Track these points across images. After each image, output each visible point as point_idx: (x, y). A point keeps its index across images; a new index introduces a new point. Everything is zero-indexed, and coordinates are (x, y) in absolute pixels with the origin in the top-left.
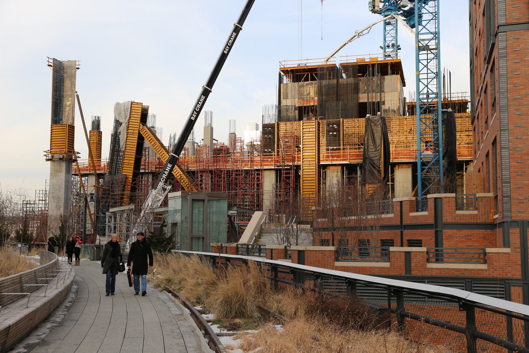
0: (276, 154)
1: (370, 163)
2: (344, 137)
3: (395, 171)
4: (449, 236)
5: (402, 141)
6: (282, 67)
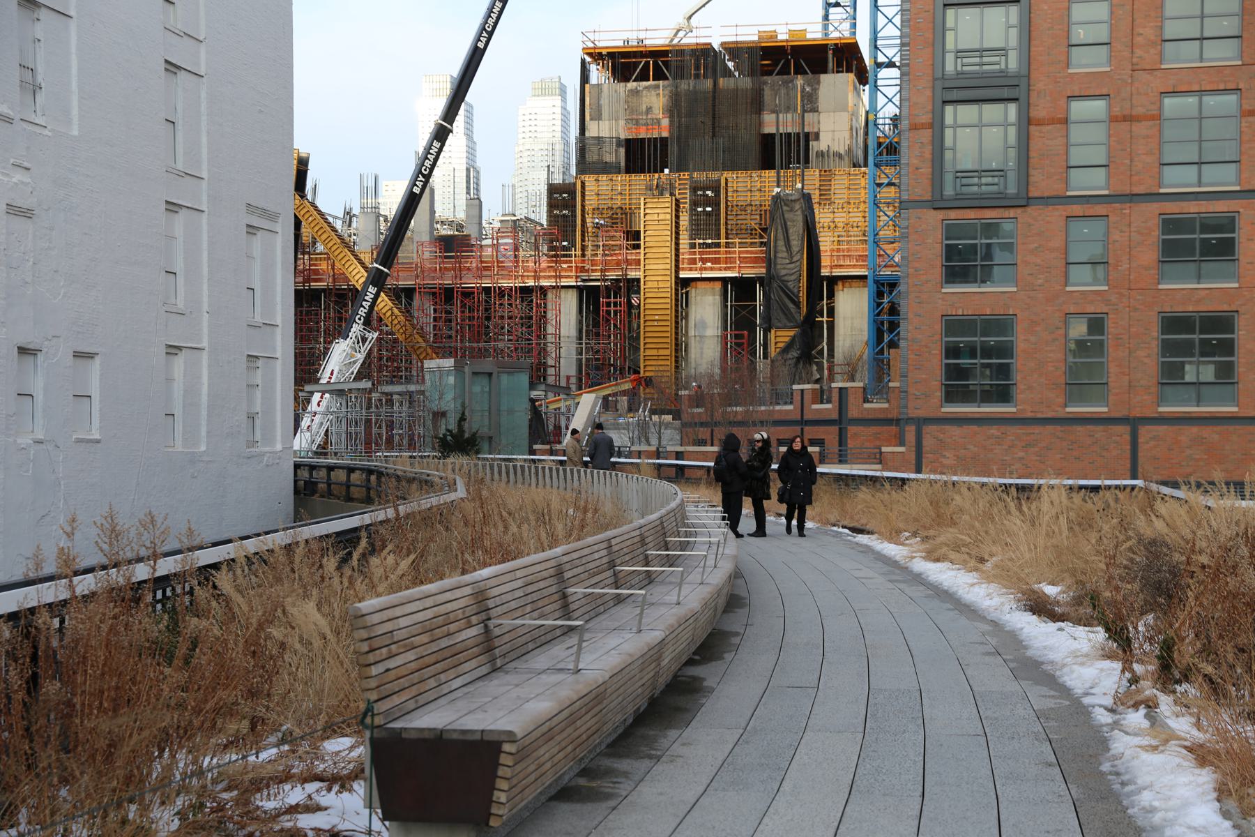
0: (579, 253)
1: (780, 287)
2: (729, 213)
3: (836, 293)
4: (855, 434)
5: (855, 224)
6: (591, 45)
